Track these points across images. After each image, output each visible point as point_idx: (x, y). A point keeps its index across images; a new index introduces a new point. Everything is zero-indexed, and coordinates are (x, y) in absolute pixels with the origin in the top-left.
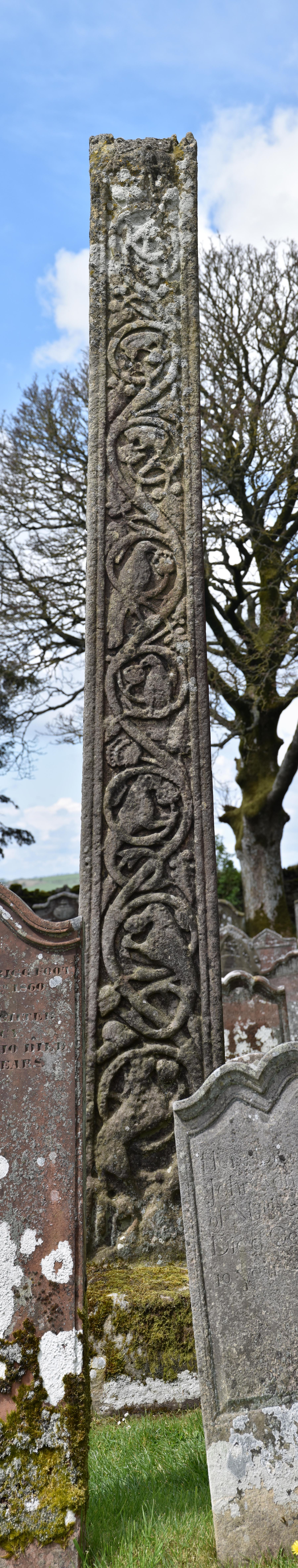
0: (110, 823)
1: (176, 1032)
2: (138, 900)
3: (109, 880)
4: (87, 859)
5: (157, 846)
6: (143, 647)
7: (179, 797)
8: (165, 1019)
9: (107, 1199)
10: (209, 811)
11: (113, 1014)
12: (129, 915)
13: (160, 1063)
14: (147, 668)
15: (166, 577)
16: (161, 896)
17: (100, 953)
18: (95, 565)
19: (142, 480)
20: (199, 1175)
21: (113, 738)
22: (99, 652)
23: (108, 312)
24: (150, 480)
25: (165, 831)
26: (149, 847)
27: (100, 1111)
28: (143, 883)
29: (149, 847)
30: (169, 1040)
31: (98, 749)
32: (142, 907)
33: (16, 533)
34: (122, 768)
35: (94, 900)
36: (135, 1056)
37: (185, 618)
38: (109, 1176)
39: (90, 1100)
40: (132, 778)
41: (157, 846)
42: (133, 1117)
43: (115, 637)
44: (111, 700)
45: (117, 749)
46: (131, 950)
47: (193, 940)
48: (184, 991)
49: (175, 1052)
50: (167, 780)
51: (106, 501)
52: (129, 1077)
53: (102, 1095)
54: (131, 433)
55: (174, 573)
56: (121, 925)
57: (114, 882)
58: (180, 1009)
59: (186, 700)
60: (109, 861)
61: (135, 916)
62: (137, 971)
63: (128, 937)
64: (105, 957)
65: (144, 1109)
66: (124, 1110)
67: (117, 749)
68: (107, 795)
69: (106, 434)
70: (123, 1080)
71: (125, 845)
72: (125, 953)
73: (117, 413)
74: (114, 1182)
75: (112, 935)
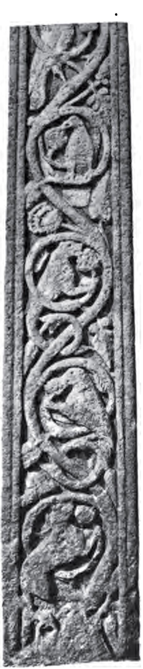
1: (93, 484)
3: (30, 344)
7: (100, 263)
10: (129, 280)
14: (69, 131)
16: (80, 360)
26: (70, 312)
27: (24, 545)
29: (70, 312)
30: (86, 490)
31: (20, 215)
34: (44, 234)
36: (55, 502)
37: (108, 77)
39: (14, 537)
40: (52, 247)
41: (77, 312)
43: (38, 94)
44: (33, 166)
49: (92, 499)
50: (89, 246)
53: (26, 533)
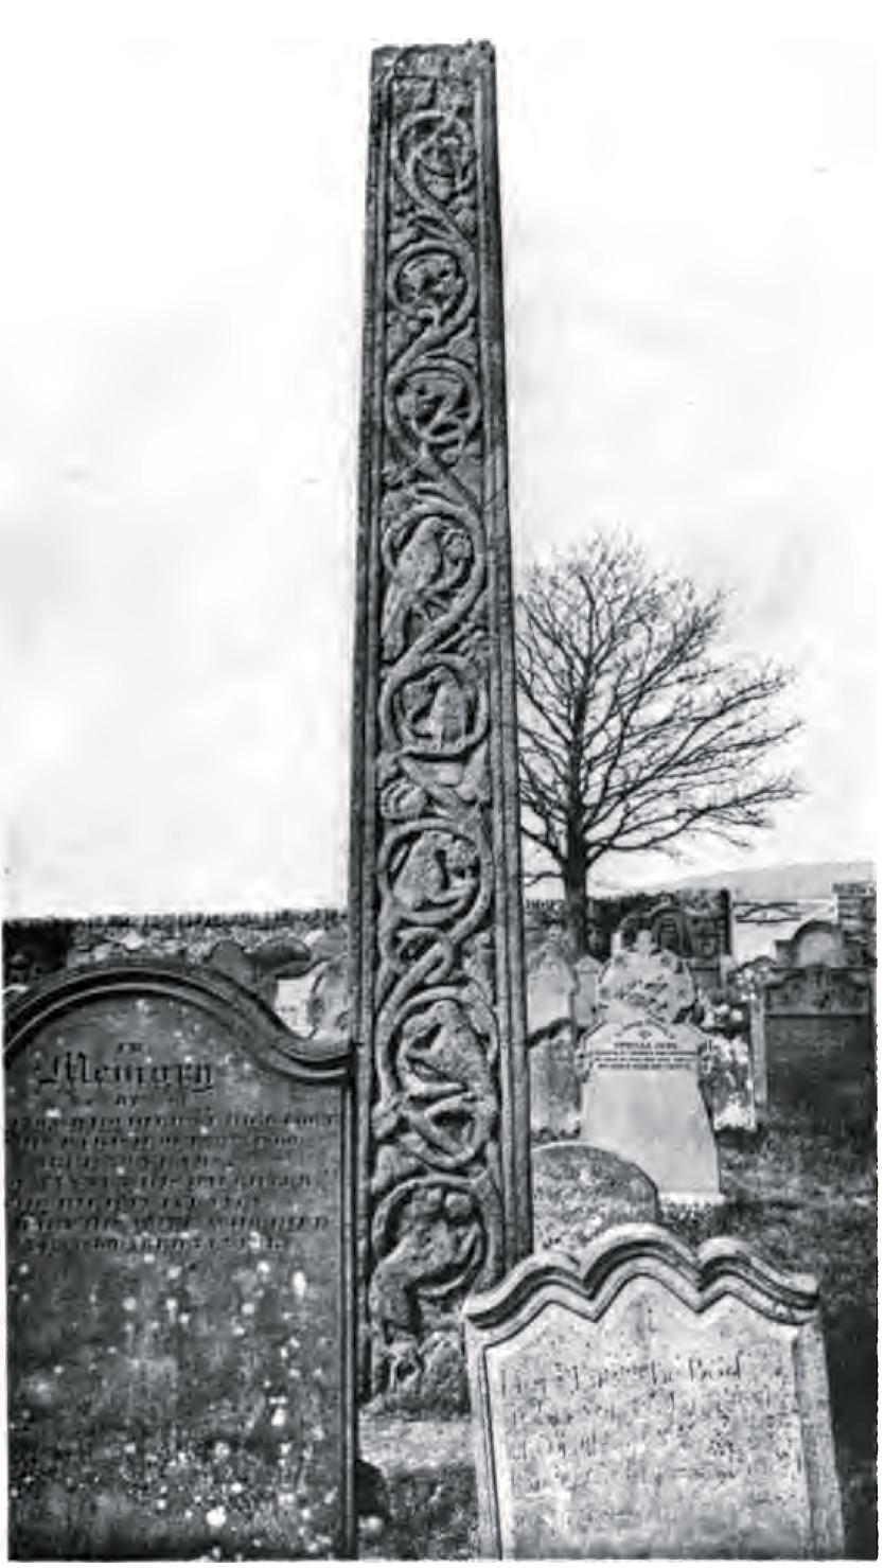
5: (446, 925)
7: (477, 859)
8: (453, 1146)
9: (384, 1348)
11: (391, 1138)
15: (461, 564)
19: (432, 439)
20: (503, 1463)
21: (388, 781)
24: (440, 439)
30: (460, 1170)
32: (427, 1005)
40: (412, 837)
41: (446, 925)
43: (393, 639)
44: (387, 735)
47: (494, 1046)
53: (378, 1231)
54: (415, 381)
55: (471, 560)
57: (390, 971)
71: (405, 924)
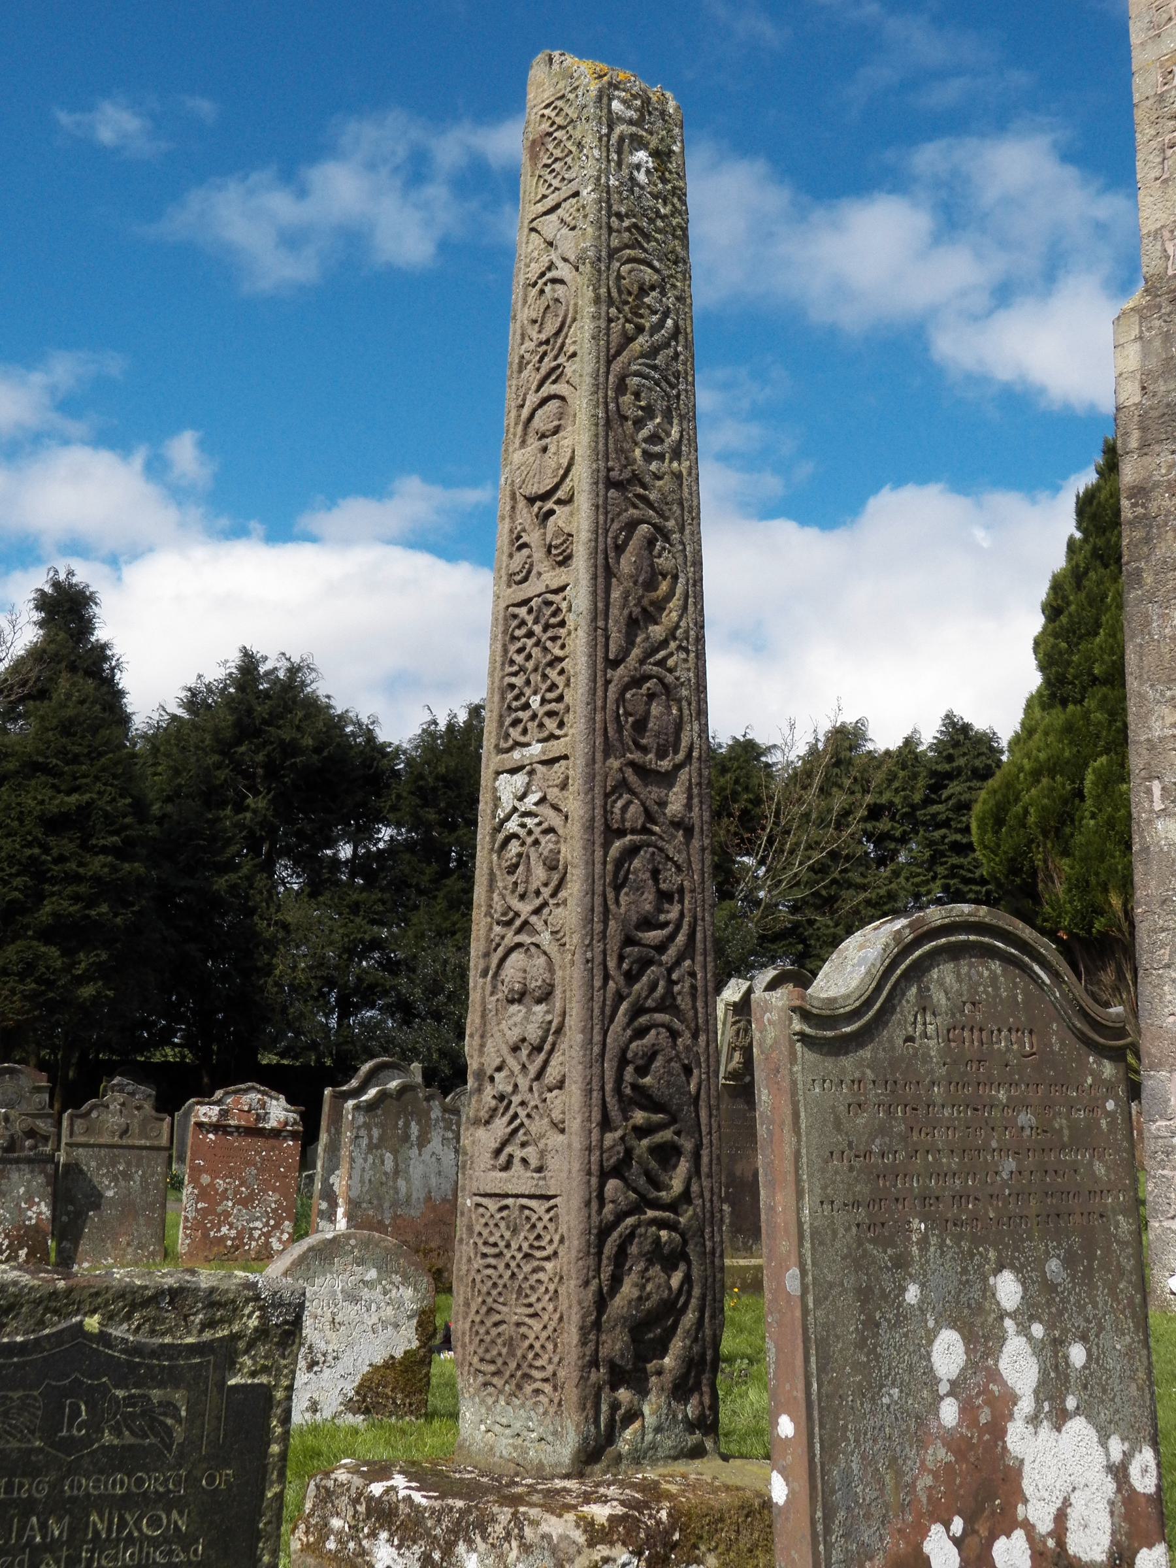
0: (612, 907)
2: (643, 1020)
4: (589, 955)
6: (647, 668)
12: (631, 1040)
13: (664, 1234)
14: (651, 696)
17: (602, 1089)
18: (596, 540)
22: (600, 666)
23: (610, 230)
25: (670, 928)
28: (647, 997)
30: (673, 1207)
33: (595, 1219)
35: (597, 1012)
38: (613, 1367)
42: (640, 1298)
43: (616, 637)
45: (619, 804)
46: (634, 1087)
48: (688, 1145)
51: (607, 460)
52: (633, 1249)
56: (624, 1051)
58: (683, 1166)
59: (689, 756)
60: (612, 964)
61: (639, 1042)
62: (639, 1117)
63: (630, 1069)
64: (608, 1099)
65: (648, 1289)
66: (628, 1289)
67: (619, 804)
68: (609, 867)
69: (608, 373)
70: (626, 1255)
72: (628, 1091)
73: (618, 353)
74: (618, 1377)
75: (615, 1064)
